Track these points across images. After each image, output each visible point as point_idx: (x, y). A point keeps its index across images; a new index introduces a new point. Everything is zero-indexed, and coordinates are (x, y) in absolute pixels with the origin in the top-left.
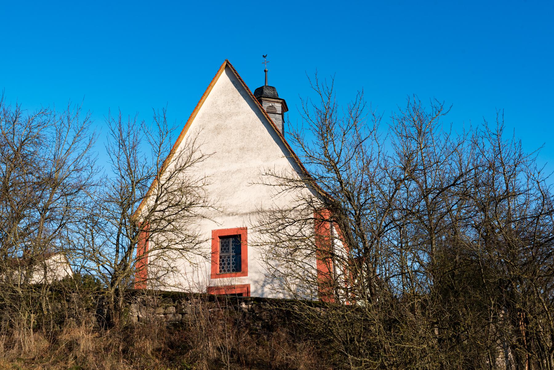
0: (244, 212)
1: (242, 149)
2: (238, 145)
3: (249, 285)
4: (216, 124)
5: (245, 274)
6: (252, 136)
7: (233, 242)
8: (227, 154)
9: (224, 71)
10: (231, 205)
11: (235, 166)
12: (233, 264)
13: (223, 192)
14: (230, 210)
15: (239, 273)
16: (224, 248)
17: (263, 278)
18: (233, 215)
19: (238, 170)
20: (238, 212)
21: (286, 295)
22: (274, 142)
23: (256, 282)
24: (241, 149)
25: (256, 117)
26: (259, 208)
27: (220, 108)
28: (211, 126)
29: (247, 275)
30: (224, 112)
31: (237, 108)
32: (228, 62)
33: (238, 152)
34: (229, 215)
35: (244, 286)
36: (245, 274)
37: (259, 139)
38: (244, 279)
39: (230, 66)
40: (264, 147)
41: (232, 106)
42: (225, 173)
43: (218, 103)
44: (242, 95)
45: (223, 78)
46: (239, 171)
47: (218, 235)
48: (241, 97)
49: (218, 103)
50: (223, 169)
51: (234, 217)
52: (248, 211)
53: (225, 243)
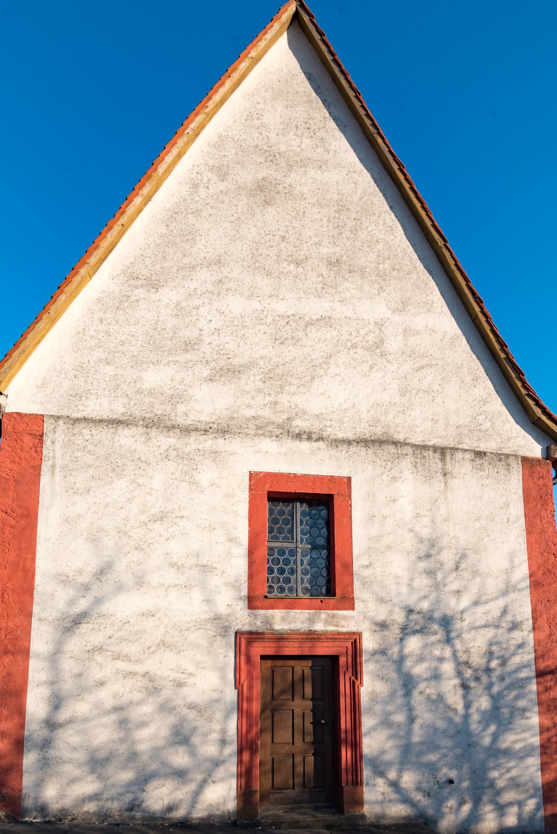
0: (340, 435)
1: (334, 263)
2: (324, 251)
3: (360, 634)
4: (260, 176)
5: (348, 603)
6: (363, 235)
7: (303, 514)
8: (292, 266)
9: (284, 39)
10: (305, 413)
11: (315, 307)
12: (305, 573)
13: (279, 371)
14: (300, 424)
15: (332, 601)
16: (279, 527)
17: (399, 617)
18: (309, 438)
19: (322, 318)
20: (325, 434)
21: (543, 681)
22: (420, 265)
23: (383, 626)
24: (330, 263)
25: (373, 187)
26: (379, 431)
27: (273, 136)
28: (247, 175)
29: (352, 608)
30: (283, 148)
31: (320, 150)
32: (302, 5)
33: (324, 270)
34: (298, 436)
35: (336, 637)
36: (348, 603)
37: (380, 247)
38: (345, 618)
39: (306, 18)
40: (395, 273)
41: (307, 142)
42: (288, 319)
43: (265, 120)
44: (336, 120)
45: (276, 59)
46: (325, 321)
47: (267, 488)
48: (332, 124)
49: (265, 120)
50: (281, 308)
51: (315, 445)
52: (350, 435)
53: (282, 513)
